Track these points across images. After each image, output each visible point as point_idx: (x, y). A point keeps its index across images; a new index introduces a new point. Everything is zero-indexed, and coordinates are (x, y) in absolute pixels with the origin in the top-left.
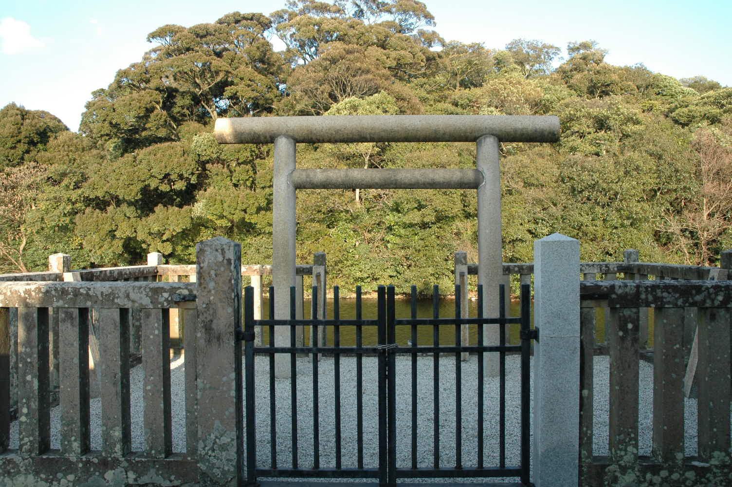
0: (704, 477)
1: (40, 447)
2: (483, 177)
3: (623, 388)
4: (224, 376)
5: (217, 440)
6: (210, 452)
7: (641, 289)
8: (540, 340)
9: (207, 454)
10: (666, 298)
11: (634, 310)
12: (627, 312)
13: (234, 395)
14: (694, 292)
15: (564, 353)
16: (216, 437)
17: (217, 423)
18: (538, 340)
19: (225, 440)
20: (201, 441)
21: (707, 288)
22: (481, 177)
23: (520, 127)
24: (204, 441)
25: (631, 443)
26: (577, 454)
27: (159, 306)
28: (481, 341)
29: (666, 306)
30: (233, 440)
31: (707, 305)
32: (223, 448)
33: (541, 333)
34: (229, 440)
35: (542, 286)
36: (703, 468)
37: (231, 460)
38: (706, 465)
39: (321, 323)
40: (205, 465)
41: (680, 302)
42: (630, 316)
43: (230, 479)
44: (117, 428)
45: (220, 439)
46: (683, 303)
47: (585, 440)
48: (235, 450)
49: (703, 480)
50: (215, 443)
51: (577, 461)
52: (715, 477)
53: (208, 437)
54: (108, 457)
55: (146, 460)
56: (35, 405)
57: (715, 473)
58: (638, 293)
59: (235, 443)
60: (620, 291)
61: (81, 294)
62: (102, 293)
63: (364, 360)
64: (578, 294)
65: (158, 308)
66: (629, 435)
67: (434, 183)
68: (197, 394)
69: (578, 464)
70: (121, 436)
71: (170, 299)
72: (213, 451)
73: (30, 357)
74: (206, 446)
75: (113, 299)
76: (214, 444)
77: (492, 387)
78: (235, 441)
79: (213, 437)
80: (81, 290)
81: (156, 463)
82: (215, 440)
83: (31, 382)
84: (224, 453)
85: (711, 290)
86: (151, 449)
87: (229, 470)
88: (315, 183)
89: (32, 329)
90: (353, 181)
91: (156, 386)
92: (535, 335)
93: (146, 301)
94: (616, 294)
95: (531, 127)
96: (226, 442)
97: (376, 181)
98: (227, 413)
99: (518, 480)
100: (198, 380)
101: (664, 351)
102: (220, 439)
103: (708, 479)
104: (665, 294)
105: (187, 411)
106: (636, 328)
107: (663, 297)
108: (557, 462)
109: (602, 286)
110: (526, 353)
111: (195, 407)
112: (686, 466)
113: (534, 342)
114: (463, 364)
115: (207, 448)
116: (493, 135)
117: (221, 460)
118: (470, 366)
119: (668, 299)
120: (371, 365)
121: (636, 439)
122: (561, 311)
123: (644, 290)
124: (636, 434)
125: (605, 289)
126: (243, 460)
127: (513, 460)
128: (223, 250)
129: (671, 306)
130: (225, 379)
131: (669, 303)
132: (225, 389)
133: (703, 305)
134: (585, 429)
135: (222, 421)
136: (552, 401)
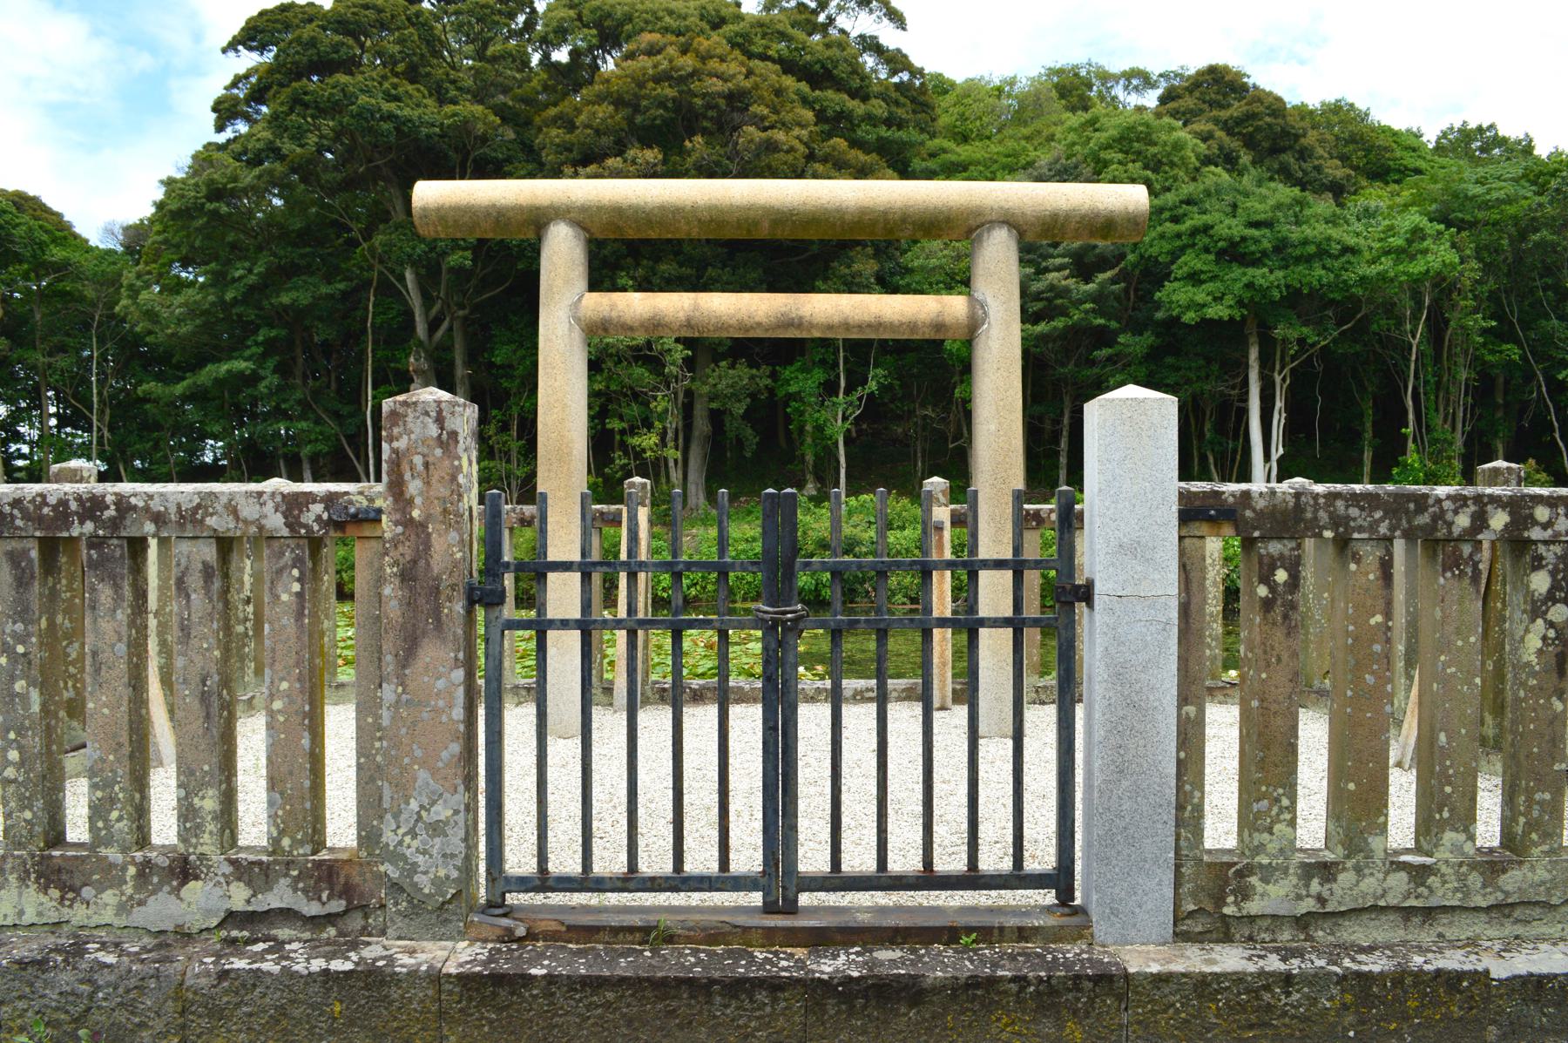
0: (1423, 884)
1: (46, 833)
2: (985, 313)
3: (1265, 705)
4: (438, 679)
5: (424, 814)
6: (408, 839)
7: (1303, 499)
8: (1097, 607)
9: (400, 843)
10: (1354, 519)
11: (1293, 544)
12: (1275, 548)
13: (462, 718)
14: (1412, 506)
15: (1144, 630)
16: (422, 807)
17: (423, 775)
18: (1090, 605)
19: (441, 812)
20: (388, 816)
21: (1439, 501)
22: (980, 312)
23: (1064, 207)
24: (396, 816)
25: (1282, 817)
26: (1172, 840)
27: (303, 531)
28: (972, 606)
29: (1356, 535)
30: (456, 812)
31: (1439, 535)
32: (437, 829)
33: (1098, 588)
34: (450, 812)
35: (1100, 490)
36: (1424, 867)
37: (453, 856)
38: (1428, 860)
39: (642, 565)
40: (396, 866)
41: (1383, 529)
42: (1282, 556)
43: (449, 896)
44: (211, 792)
45: (428, 810)
46: (1389, 529)
47: (1188, 814)
48: (462, 834)
49: (1420, 890)
50: (420, 818)
51: (1172, 855)
52: (1444, 882)
53: (403, 806)
54: (190, 854)
55: (271, 859)
56: (35, 742)
57: (1443, 875)
58: (1299, 508)
59: (461, 818)
60: (1260, 504)
61: (134, 508)
62: (179, 506)
63: (735, 711)
64: (1175, 508)
65: (301, 537)
66: (1277, 800)
67: (881, 324)
68: (381, 717)
69: (1173, 861)
70: (218, 808)
71: (325, 516)
72: (415, 836)
73: (23, 643)
74: (398, 827)
75: (203, 518)
76: (417, 821)
77: (998, 754)
78: (462, 814)
79: (414, 805)
80: (133, 500)
81: (291, 866)
82: (418, 813)
83: (25, 698)
84: (437, 840)
85: (1447, 505)
86: (282, 833)
87: (447, 877)
88: (629, 322)
89: (27, 584)
90: (710, 319)
91: (291, 702)
92: (1086, 594)
93: (276, 522)
94: (1254, 510)
95: (1086, 206)
96: (442, 818)
97: (757, 319)
98: (445, 755)
99: (1048, 897)
100: (384, 685)
101: (1351, 628)
102: (428, 810)
103: (1429, 888)
104: (1354, 512)
105: (360, 754)
106: (1294, 582)
107: (1348, 518)
108: (1129, 856)
109: (1224, 493)
110: (1067, 696)
111: (377, 744)
112: (1392, 863)
113: (1081, 607)
114: (937, 715)
115: (400, 832)
116: (1003, 222)
117: (431, 856)
118: (951, 724)
119: (1360, 522)
120: (748, 722)
121: (1292, 809)
122: (1139, 543)
123: (1312, 502)
124: (1294, 802)
125: (1231, 499)
126: (478, 857)
127: (1041, 857)
128: (440, 412)
129: (1365, 536)
130: (441, 684)
131: (1360, 529)
132: (441, 703)
133: (1431, 534)
134: (1188, 787)
135: (434, 772)
136: (1121, 729)
